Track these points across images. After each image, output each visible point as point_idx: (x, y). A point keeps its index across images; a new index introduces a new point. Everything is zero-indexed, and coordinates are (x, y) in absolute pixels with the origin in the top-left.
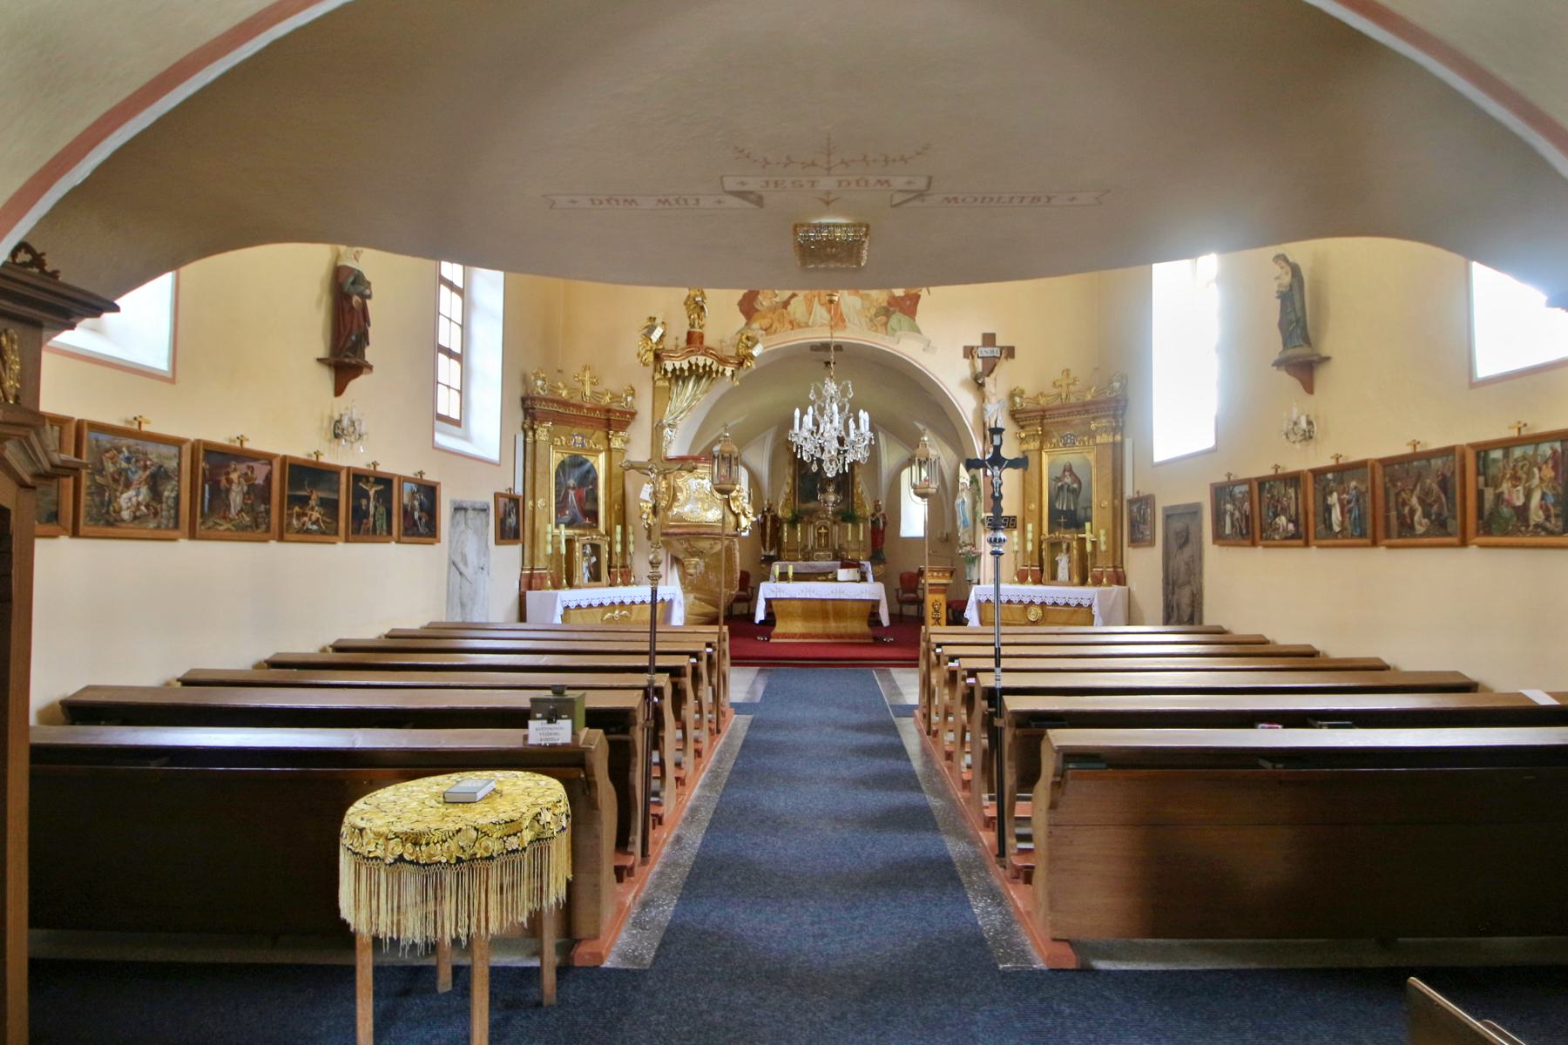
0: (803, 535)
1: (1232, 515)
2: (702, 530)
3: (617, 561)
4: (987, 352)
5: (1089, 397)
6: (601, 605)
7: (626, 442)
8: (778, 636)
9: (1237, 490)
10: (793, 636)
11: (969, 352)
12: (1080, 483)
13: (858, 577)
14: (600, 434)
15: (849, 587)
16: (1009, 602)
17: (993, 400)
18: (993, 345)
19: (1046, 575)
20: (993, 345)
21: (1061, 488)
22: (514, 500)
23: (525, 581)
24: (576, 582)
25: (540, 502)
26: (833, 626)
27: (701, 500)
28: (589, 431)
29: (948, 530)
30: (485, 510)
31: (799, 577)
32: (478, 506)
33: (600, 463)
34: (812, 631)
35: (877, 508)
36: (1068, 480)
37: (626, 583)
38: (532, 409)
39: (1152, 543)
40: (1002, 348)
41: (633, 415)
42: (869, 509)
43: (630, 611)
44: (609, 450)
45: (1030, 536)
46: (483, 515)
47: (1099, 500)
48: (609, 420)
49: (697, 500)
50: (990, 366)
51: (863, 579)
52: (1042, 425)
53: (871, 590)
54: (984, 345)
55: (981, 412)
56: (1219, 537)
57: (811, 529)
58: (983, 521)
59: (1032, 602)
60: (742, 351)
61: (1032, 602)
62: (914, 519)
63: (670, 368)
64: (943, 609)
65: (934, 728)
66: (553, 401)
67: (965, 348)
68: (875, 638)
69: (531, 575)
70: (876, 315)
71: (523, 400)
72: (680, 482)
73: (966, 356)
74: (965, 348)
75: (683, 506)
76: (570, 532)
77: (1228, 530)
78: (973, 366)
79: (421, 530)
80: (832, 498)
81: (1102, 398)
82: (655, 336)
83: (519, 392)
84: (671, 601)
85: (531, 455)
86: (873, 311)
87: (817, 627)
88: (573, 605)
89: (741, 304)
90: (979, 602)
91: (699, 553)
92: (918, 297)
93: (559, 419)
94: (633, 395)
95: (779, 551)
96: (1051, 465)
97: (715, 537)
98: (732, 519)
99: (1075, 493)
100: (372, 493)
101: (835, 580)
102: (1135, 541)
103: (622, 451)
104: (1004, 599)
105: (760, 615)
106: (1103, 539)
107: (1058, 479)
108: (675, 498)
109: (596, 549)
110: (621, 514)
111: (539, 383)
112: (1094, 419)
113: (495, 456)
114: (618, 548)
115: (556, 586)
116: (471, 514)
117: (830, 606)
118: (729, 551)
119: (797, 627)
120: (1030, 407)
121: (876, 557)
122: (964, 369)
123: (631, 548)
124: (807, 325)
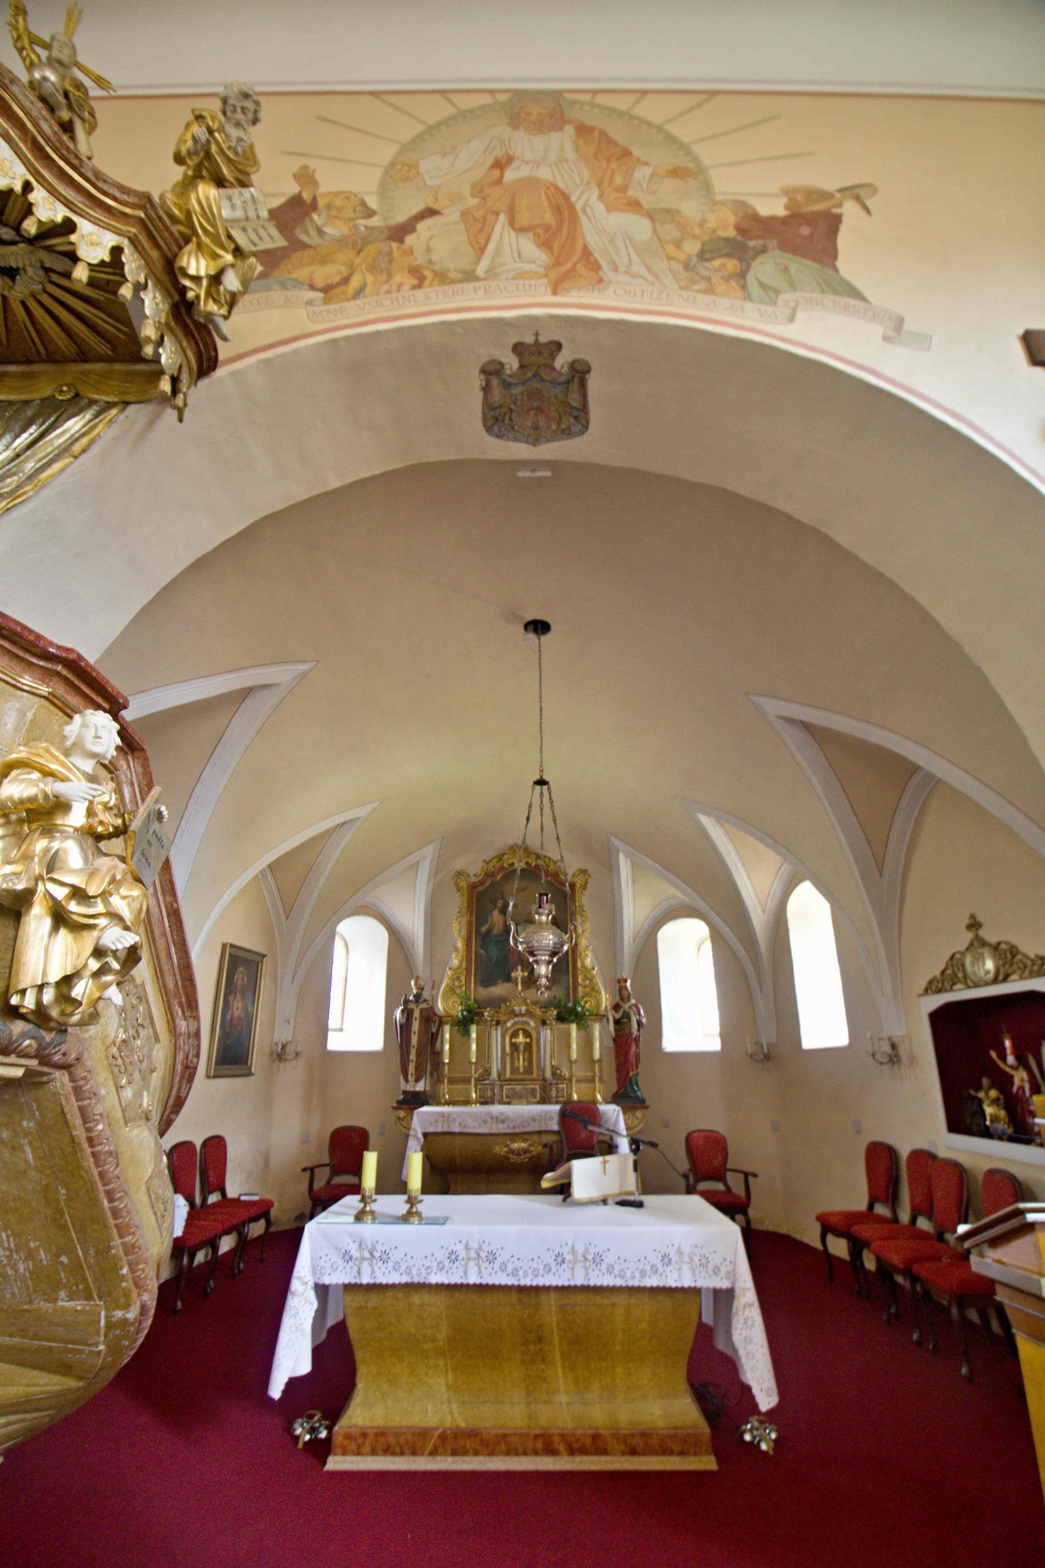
10: (414, 1442)
29: (768, 1035)
35: (622, 994)
42: (605, 1000)
57: (496, 1035)
62: (691, 1017)
70: (702, 256)
86: (692, 247)
92: (837, 219)
105: (293, 1357)
117: (550, 1314)
124: (469, 276)
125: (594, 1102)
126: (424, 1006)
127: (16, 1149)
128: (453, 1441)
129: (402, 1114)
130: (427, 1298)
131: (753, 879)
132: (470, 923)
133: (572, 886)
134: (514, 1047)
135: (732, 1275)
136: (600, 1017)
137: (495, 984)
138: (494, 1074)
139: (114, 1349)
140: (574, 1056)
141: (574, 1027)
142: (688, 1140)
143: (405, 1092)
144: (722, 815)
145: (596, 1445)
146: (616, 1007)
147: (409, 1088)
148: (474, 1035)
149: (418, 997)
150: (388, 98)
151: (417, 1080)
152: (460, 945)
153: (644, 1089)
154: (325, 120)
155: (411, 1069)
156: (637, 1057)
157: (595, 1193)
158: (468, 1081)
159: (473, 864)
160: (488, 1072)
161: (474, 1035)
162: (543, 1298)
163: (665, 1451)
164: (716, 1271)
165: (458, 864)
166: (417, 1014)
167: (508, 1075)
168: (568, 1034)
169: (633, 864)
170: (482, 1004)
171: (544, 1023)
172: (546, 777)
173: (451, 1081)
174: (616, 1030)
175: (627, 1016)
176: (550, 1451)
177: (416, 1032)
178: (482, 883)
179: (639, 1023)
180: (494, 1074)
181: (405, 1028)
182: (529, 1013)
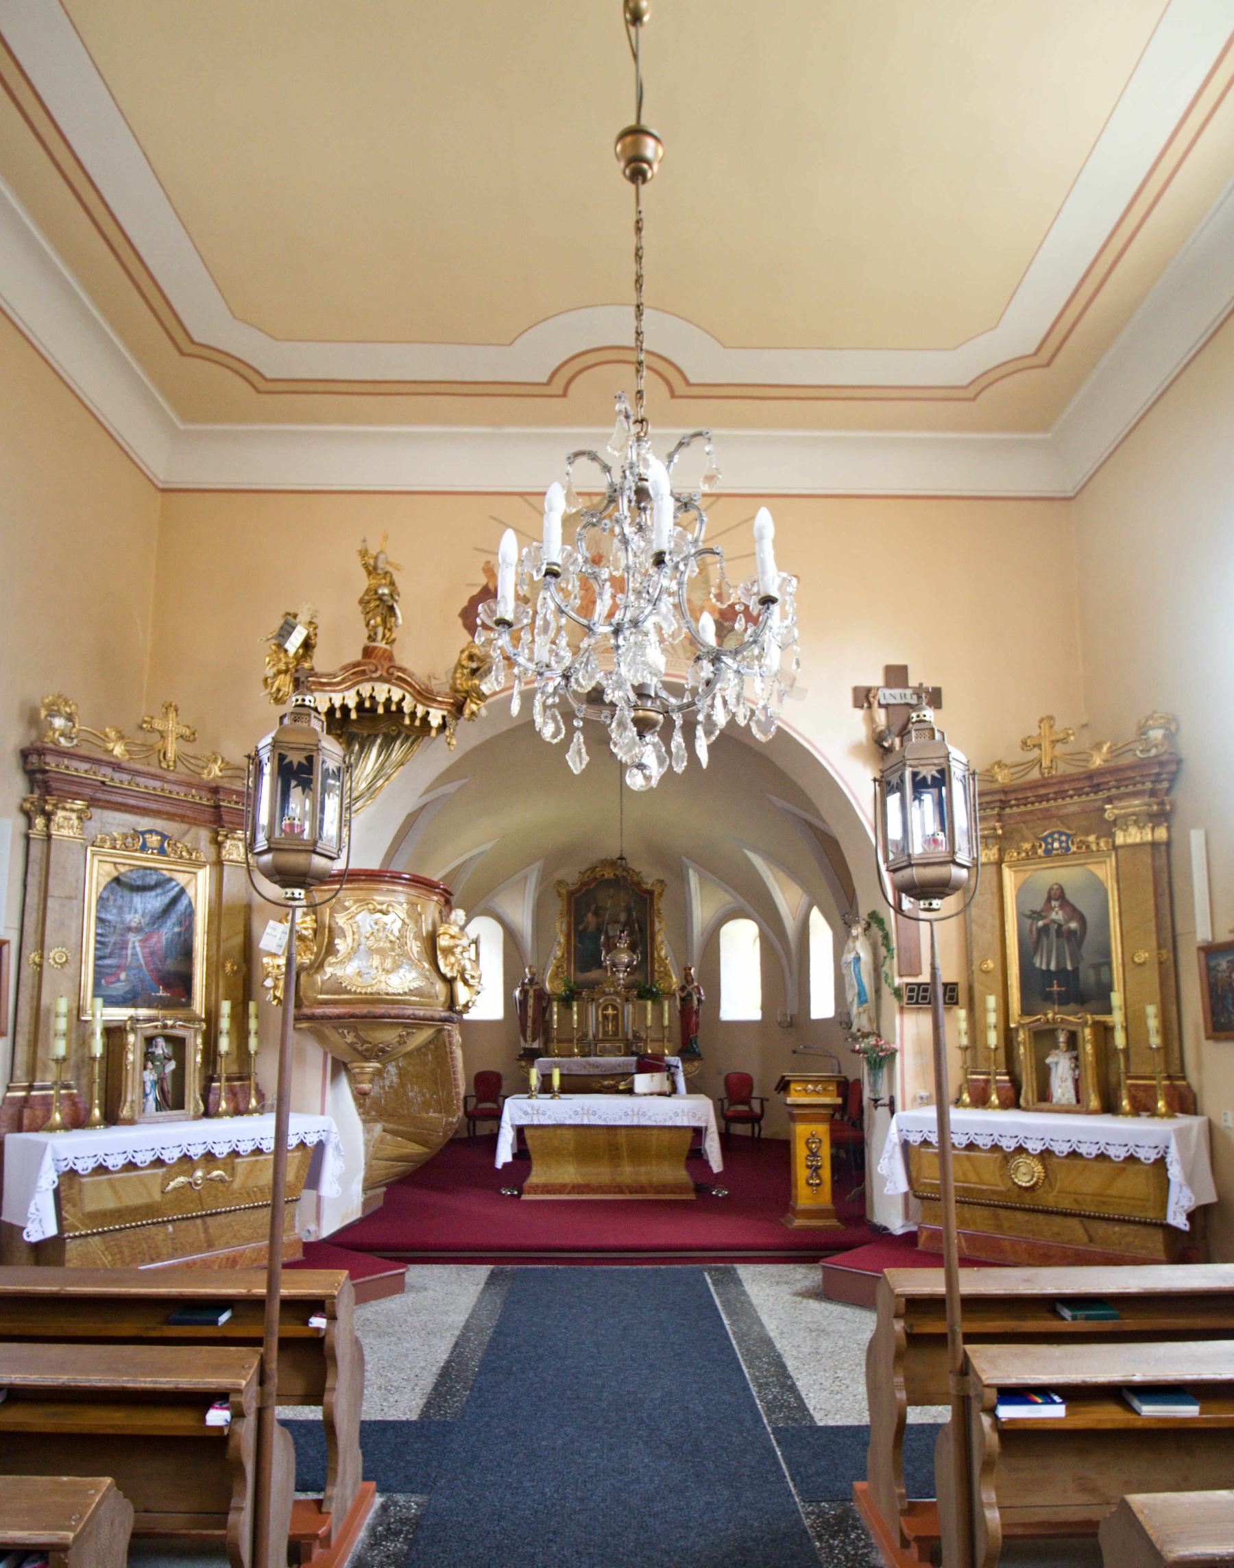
0: (586, 1017)
2: (380, 1009)
3: (225, 1067)
4: (893, 695)
5: (1097, 761)
6: (159, 1162)
8: (536, 1189)
10: (561, 1188)
11: (863, 697)
12: (1082, 919)
13: (667, 1087)
14: (204, 835)
15: (663, 1105)
16: (971, 1146)
18: (905, 685)
20: (905, 685)
21: (1045, 930)
24: (125, 1112)
25: (55, 955)
26: (628, 1172)
27: (381, 952)
29: (792, 1009)
31: (573, 1085)
35: (687, 979)
36: (1057, 915)
42: (675, 981)
43: (232, 1171)
44: (219, 863)
49: (371, 951)
52: (1000, 818)
53: (692, 1110)
57: (592, 1009)
58: (897, 992)
59: (1021, 1150)
60: (462, 684)
61: (1021, 1150)
62: (741, 996)
64: (826, 1151)
67: (856, 690)
69: (26, 1100)
71: (25, 755)
72: (341, 919)
74: (856, 690)
76: (120, 1014)
78: (871, 720)
80: (625, 958)
81: (1127, 760)
82: (294, 643)
84: (321, 1145)
87: (601, 1173)
88: (85, 1165)
90: (905, 1145)
91: (379, 1053)
95: (547, 1041)
96: (1021, 891)
97: (419, 1022)
98: (440, 987)
99: (1075, 939)
101: (630, 1091)
104: (959, 1140)
105: (504, 1154)
107: (1036, 915)
108: (331, 950)
109: (178, 1044)
111: (59, 722)
112: (1109, 800)
115: (78, 1121)
117: (622, 1137)
118: (439, 1045)
119: (568, 1173)
121: (688, 1051)
122: (855, 726)
123: (253, 1043)
125: (664, 1055)
126: (536, 987)
127: (426, 1055)
129: (523, 1064)
130: (565, 1132)
131: (787, 899)
132: (569, 923)
133: (651, 893)
134: (605, 1017)
135: (707, 1121)
136: (671, 995)
137: (589, 971)
138: (591, 1036)
139: (445, 1133)
140: (649, 1023)
141: (649, 1003)
142: (727, 1080)
143: (524, 1049)
144: (768, 856)
145: (642, 1189)
146: (683, 989)
147: (527, 1046)
148: (575, 1009)
149: (531, 980)
150: (528, 498)
151: (534, 1040)
152: (562, 940)
153: (701, 1046)
154: (495, 519)
155: (529, 1033)
156: (697, 1024)
157: (646, 1090)
158: (571, 1041)
159: (571, 874)
160: (586, 1035)
161: (575, 1009)
162: (619, 1131)
163: (673, 1192)
164: (699, 1119)
165: (559, 875)
166: (531, 993)
167: (601, 1036)
168: (646, 1008)
169: (700, 877)
171: (627, 1000)
172: (625, 856)
173: (559, 1041)
174: (682, 1006)
175: (690, 995)
176: (622, 1192)
177: (531, 1009)
178: (578, 890)
179: (699, 1000)
180: (591, 1036)
181: (523, 1003)
182: (616, 993)
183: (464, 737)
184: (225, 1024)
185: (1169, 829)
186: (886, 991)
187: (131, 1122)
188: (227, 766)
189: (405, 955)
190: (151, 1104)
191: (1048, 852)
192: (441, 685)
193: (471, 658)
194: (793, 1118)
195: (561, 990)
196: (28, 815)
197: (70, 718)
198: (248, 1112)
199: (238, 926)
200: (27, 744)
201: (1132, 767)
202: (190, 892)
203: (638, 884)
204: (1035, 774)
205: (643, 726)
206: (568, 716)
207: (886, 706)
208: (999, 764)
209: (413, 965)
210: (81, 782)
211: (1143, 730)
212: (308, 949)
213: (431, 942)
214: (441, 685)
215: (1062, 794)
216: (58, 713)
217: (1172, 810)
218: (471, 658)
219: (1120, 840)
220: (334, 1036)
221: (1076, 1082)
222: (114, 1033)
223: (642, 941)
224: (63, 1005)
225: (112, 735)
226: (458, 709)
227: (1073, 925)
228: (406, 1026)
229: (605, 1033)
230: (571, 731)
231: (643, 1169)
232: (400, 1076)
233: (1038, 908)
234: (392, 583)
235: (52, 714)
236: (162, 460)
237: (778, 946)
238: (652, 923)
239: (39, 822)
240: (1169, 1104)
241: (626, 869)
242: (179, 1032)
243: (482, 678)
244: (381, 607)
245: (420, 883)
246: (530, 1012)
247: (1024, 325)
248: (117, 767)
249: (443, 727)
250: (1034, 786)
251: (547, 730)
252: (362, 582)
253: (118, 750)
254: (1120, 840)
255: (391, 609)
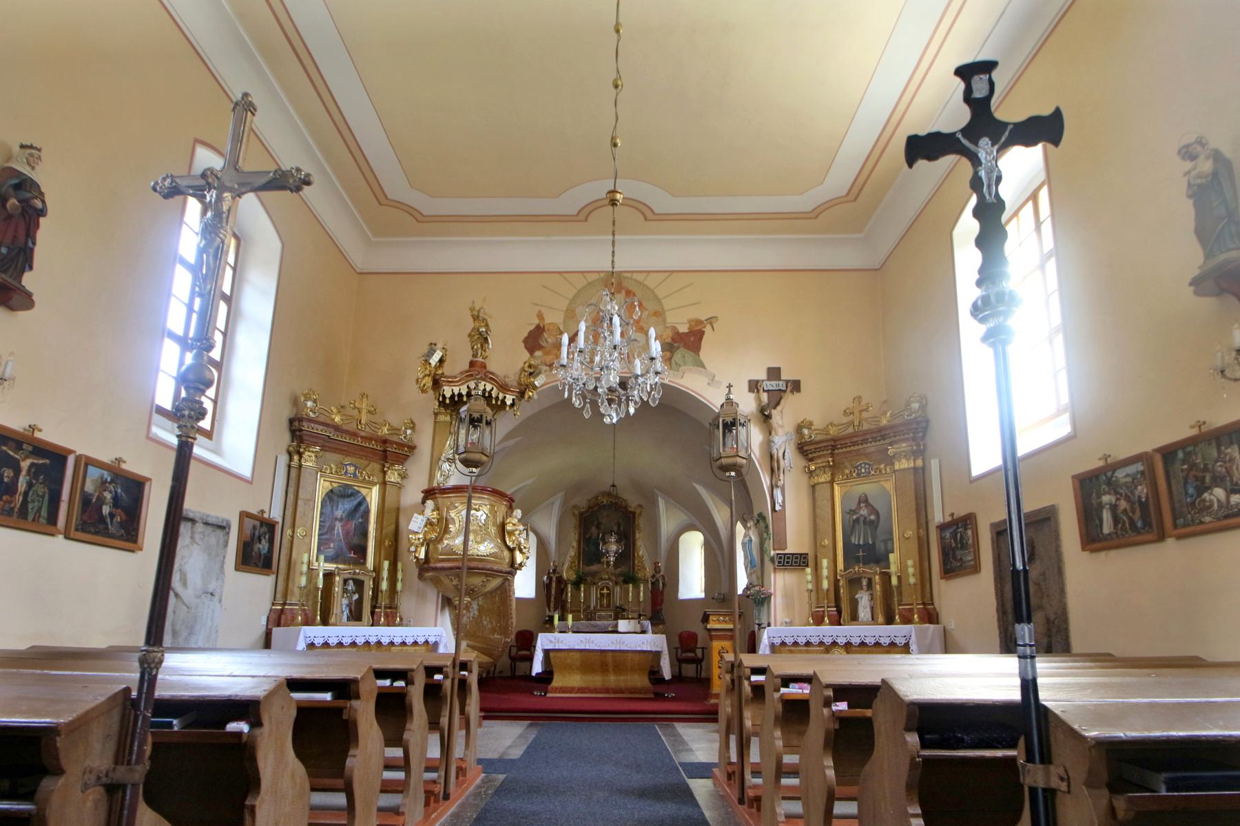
1: (1114, 508)
3: (383, 601)
4: (772, 385)
5: (884, 422)
7: (404, 476)
9: (1120, 474)
10: (571, 690)
12: (877, 514)
14: (376, 466)
15: (633, 638)
17: (780, 431)
19: (845, 614)
21: (857, 520)
22: (270, 526)
23: (274, 616)
24: (333, 620)
26: (612, 680)
28: (364, 462)
29: (725, 590)
30: (223, 527)
32: (211, 520)
33: (373, 497)
34: (591, 685)
36: (864, 512)
37: (390, 623)
38: (298, 432)
39: (976, 569)
40: (787, 382)
41: (412, 448)
42: (649, 571)
44: (384, 484)
45: (825, 572)
46: (219, 533)
47: (901, 530)
48: (385, 451)
50: (776, 398)
51: (643, 632)
52: (832, 455)
53: (652, 641)
54: (769, 379)
55: (768, 444)
56: (1092, 539)
57: (593, 590)
58: (772, 560)
62: (692, 583)
63: (448, 395)
65: (750, 793)
66: (327, 425)
67: (750, 381)
68: (656, 694)
69: (282, 610)
71: (291, 421)
72: (453, 514)
73: (751, 390)
74: (750, 381)
75: (453, 538)
76: (331, 567)
77: (1107, 527)
78: (759, 399)
79: (112, 529)
80: (614, 548)
81: (897, 421)
82: (434, 360)
83: (287, 413)
85: (295, 476)
87: (596, 680)
89: (526, 341)
92: (703, 333)
93: (328, 445)
94: (413, 428)
98: (506, 553)
99: (873, 525)
100: (25, 465)
102: (949, 571)
103: (399, 487)
105: (537, 668)
106: (911, 570)
107: (852, 512)
109: (359, 584)
110: (393, 545)
111: (309, 404)
112: (891, 444)
113: (245, 470)
114: (384, 585)
115: (308, 622)
116: (200, 527)
120: (819, 438)
123: (399, 586)
128: (581, 690)
131: (720, 515)
133: (634, 513)
134: (602, 595)
136: (646, 581)
144: (707, 486)
146: (653, 576)
149: (554, 571)
152: (575, 544)
159: (582, 501)
160: (589, 607)
165: (575, 501)
169: (667, 503)
170: (586, 575)
177: (553, 591)
181: (548, 586)
182: (609, 579)
183: (524, 411)
184: (385, 574)
185: (923, 460)
186: (767, 559)
187: (335, 625)
188: (392, 428)
189: (488, 534)
190: (345, 617)
191: (858, 475)
192: (512, 380)
193: (530, 366)
194: (711, 638)
195: (573, 577)
196: (290, 454)
197: (315, 401)
198: (394, 625)
199: (393, 517)
200: (292, 416)
201: (901, 425)
202: (368, 499)
203: (626, 507)
204: (851, 430)
205: (610, 401)
206: (584, 398)
207: (768, 391)
208: (831, 424)
209: (492, 541)
210: (317, 436)
211: (908, 404)
212: (434, 530)
213: (502, 528)
214: (512, 380)
215: (865, 441)
216: (310, 399)
217: (924, 450)
218: (530, 366)
219: (897, 467)
220: (446, 581)
221: (872, 608)
222: (329, 576)
223: (627, 538)
224: (305, 559)
225: (335, 410)
226: (522, 394)
227: (873, 517)
228: (487, 575)
229: (602, 606)
230: (585, 403)
231: (622, 678)
232: (479, 610)
233: (854, 507)
234: (487, 325)
235: (306, 400)
236: (359, 257)
237: (714, 545)
238: (634, 533)
239: (296, 458)
240: (919, 617)
241: (617, 497)
242: (361, 577)
243: (535, 377)
244: (481, 338)
245: (495, 492)
246: (553, 592)
247: (839, 180)
248: (337, 428)
249: (512, 405)
250: (850, 436)
251: (577, 402)
252: (470, 324)
253: (337, 419)
254: (897, 467)
255: (486, 339)
